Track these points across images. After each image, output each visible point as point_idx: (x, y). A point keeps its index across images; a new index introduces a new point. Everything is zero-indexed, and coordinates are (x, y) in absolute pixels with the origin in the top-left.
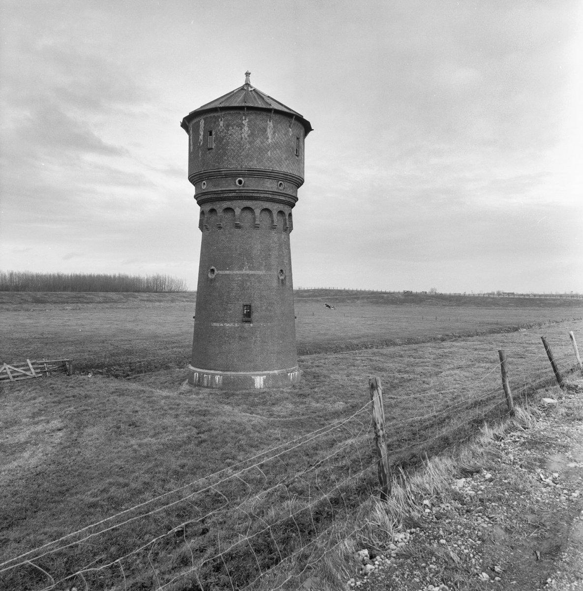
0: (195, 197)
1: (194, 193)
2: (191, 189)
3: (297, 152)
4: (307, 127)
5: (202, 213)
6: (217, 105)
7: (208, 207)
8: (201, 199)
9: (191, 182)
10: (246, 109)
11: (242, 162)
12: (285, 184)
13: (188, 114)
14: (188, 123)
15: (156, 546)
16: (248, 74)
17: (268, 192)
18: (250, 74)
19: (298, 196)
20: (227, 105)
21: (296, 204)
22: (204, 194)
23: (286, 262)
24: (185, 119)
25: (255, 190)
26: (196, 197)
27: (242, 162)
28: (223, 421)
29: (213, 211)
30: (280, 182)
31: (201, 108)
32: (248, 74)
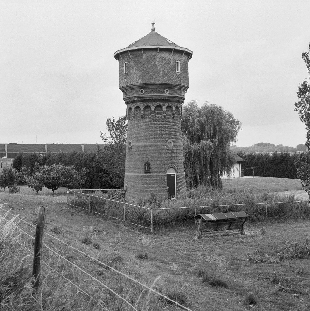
0: (298, 96)
14: (117, 56)
16: (153, 24)
18: (152, 24)
19: (185, 97)
30: (141, 90)
32: (153, 24)
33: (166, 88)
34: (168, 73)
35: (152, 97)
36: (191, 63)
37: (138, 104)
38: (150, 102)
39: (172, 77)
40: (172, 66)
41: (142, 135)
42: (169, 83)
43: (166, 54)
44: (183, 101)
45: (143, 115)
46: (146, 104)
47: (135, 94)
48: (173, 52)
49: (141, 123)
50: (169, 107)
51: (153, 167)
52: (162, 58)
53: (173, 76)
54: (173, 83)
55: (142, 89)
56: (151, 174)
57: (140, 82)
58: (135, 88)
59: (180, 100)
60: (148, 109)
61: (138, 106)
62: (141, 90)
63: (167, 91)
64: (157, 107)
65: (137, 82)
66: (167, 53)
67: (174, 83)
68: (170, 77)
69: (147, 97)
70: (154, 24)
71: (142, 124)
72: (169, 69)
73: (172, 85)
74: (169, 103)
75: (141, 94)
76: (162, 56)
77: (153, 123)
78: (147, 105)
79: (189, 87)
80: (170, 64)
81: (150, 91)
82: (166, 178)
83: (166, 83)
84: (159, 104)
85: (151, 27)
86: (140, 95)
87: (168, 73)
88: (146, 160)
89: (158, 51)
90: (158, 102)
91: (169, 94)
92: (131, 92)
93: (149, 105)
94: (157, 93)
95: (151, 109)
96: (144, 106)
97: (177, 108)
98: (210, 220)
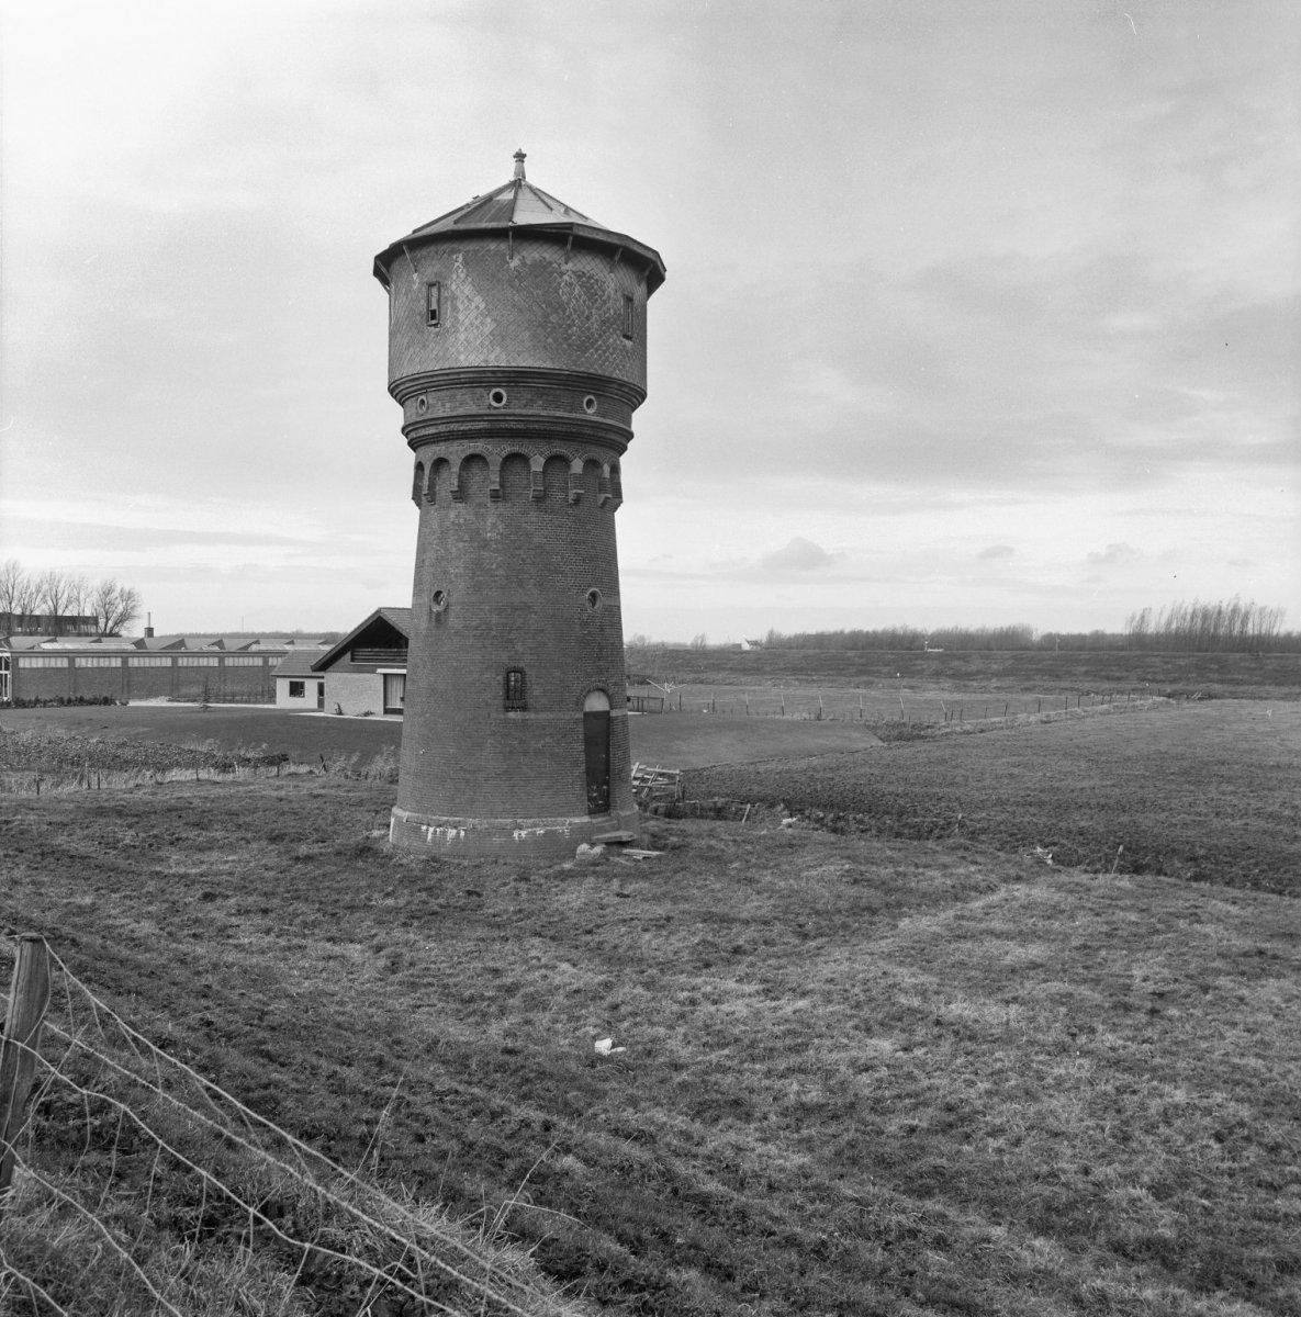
0: (403, 429)
1: (401, 423)
2: (395, 415)
3: (633, 328)
4: (646, 268)
5: (419, 467)
6: (448, 225)
7: (431, 453)
8: (415, 436)
9: (395, 398)
10: (511, 233)
11: (529, 357)
12: (430, 398)
13: (387, 247)
14: (387, 265)
15: (286, 1249)
16: (520, 157)
17: (429, 423)
18: (524, 156)
19: (634, 428)
20: (473, 226)
21: (629, 445)
22: (426, 423)
23: (323, 724)
24: (378, 258)
25: (509, 415)
26: (406, 431)
27: (529, 357)
28: (349, 1065)
29: (440, 463)
30: (494, 391)
31: (415, 232)
32: (520, 157)
33: (589, 393)
34: (600, 336)
35: (537, 419)
36: (658, 307)
37: (479, 446)
38: (526, 441)
39: (612, 354)
40: (612, 311)
41: (494, 567)
42: (600, 372)
43: (584, 261)
44: (623, 442)
45: (498, 488)
46: (508, 448)
47: (442, 406)
48: (617, 258)
49: (491, 520)
50: (557, 461)
51: (535, 691)
52: (580, 275)
53: (615, 349)
54: (614, 376)
55: (500, 387)
56: (531, 715)
57: (497, 358)
58: (420, 390)
59: (427, 433)
60: (517, 467)
61: (478, 451)
62: (494, 391)
63: (590, 403)
64: (552, 460)
65: (482, 357)
66: (597, 261)
67: (617, 374)
68: (605, 352)
69: (520, 418)
70: (524, 156)
71: (492, 522)
72: (604, 322)
73: (610, 381)
74: (593, 448)
75: (495, 408)
76: (579, 266)
77: (533, 519)
78: (516, 449)
79: (649, 392)
80: (605, 302)
81: (529, 396)
82: (580, 728)
83: (592, 371)
84: (559, 448)
85: (512, 164)
86: (494, 412)
87: (600, 336)
88: (510, 658)
89: (569, 247)
90: (556, 443)
91: (597, 413)
92: (453, 397)
93: (524, 451)
94: (557, 408)
95: (529, 467)
96: (504, 454)
97: (592, 464)
98: (331, 668)
